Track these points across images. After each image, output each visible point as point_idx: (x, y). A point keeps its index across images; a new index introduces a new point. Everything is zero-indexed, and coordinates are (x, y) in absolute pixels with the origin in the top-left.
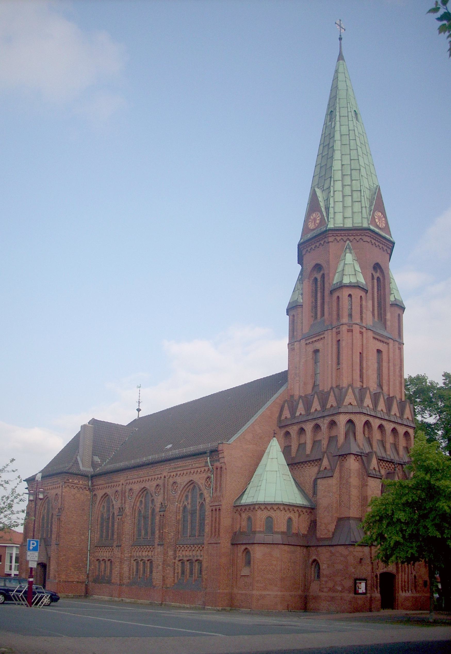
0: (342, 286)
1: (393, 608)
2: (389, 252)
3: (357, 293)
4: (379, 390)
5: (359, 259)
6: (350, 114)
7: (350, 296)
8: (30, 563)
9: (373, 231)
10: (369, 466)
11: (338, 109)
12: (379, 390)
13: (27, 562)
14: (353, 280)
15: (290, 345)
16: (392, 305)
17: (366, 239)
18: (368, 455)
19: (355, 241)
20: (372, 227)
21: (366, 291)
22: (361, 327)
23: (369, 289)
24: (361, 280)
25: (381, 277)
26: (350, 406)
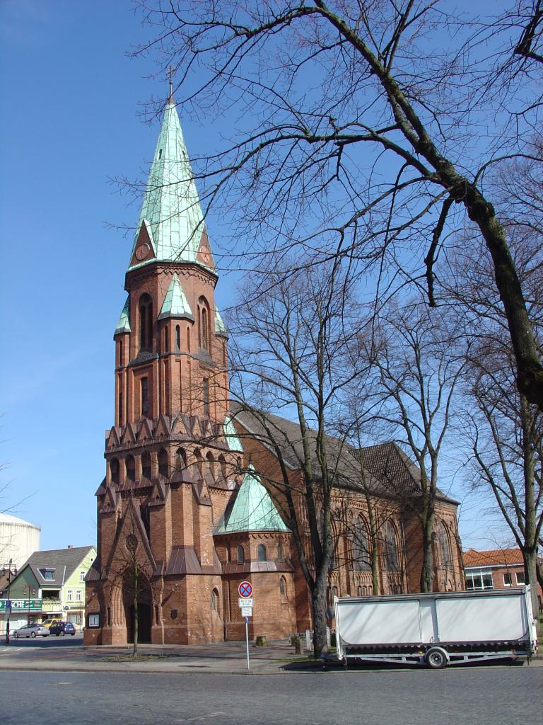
0: (169, 318)
1: (150, 643)
2: (214, 285)
3: (184, 325)
4: (207, 418)
5: (184, 291)
6: (178, 153)
7: (178, 327)
8: (243, 611)
9: (198, 265)
10: (200, 494)
11: (167, 148)
12: (207, 418)
13: (240, 610)
14: (181, 312)
15: (234, 191)
16: (216, 336)
17: (191, 272)
18: (200, 482)
19: (181, 275)
20: (197, 262)
21: (193, 322)
22: (189, 356)
23: (196, 319)
24: (189, 311)
25: (206, 309)
26: (180, 435)
